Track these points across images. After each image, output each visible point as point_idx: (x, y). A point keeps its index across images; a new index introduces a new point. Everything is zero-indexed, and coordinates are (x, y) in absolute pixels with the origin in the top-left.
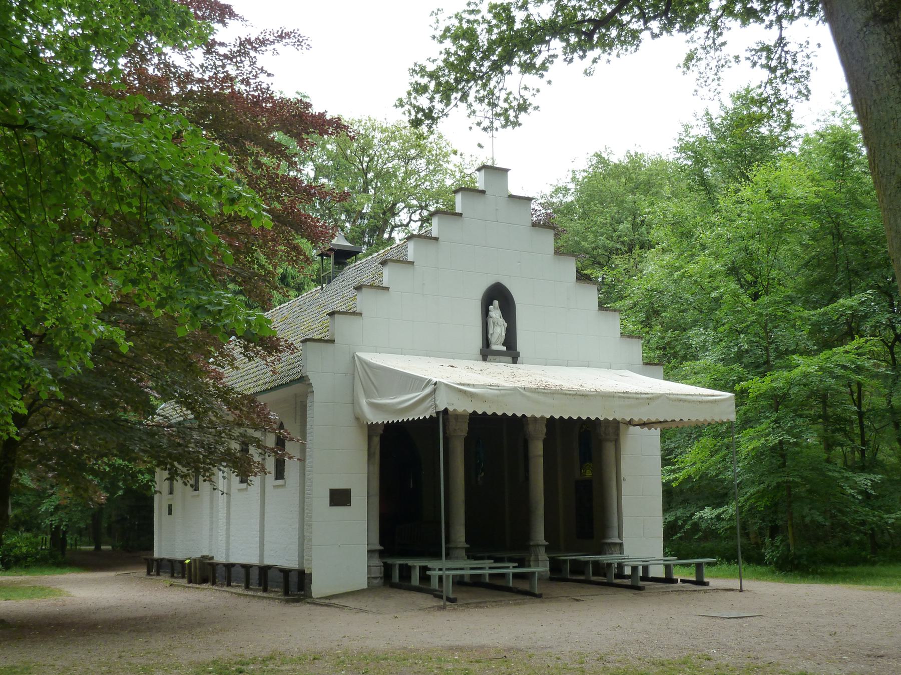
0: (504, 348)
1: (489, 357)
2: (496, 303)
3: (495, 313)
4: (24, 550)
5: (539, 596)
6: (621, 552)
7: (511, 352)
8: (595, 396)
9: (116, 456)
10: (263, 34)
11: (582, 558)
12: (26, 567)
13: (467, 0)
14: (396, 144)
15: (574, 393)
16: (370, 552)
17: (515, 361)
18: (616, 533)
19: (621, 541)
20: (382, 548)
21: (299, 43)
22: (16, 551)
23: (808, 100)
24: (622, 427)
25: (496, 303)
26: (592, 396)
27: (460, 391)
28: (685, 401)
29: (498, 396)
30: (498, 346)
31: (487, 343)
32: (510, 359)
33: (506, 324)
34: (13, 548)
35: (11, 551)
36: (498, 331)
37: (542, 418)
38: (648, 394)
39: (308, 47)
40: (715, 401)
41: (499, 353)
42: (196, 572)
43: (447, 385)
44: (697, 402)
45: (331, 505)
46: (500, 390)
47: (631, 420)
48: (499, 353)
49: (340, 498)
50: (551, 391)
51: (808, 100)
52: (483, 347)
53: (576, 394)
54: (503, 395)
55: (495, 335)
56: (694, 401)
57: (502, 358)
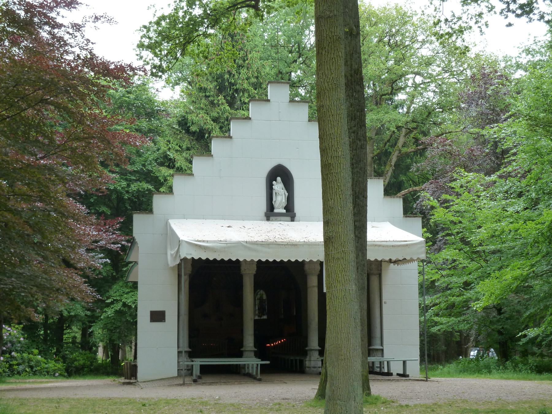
0: (284, 211)
1: (271, 218)
2: (279, 179)
3: (278, 186)
4: (81, 362)
5: (260, 380)
6: (383, 356)
8: (303, 245)
9: (520, 284)
10: (85, 19)
12: (83, 375)
15: (286, 243)
16: (179, 353)
17: (293, 220)
18: (378, 341)
19: (381, 348)
20: (190, 350)
21: (110, 20)
22: (76, 363)
24: (383, 264)
25: (279, 179)
26: (300, 245)
27: (196, 245)
28: (380, 246)
29: (225, 248)
30: (279, 209)
31: (271, 207)
32: (289, 218)
33: (287, 194)
34: (74, 361)
35: (73, 363)
36: (280, 200)
37: (252, 261)
38: (406, 241)
39: (116, 23)
40: (407, 245)
41: (280, 215)
43: (186, 242)
44: (390, 246)
45: (151, 321)
46: (227, 244)
47: (390, 260)
48: (280, 215)
50: (268, 243)
52: (267, 211)
53: (287, 245)
54: (229, 247)
55: (277, 202)
56: (387, 246)
57: (282, 218)
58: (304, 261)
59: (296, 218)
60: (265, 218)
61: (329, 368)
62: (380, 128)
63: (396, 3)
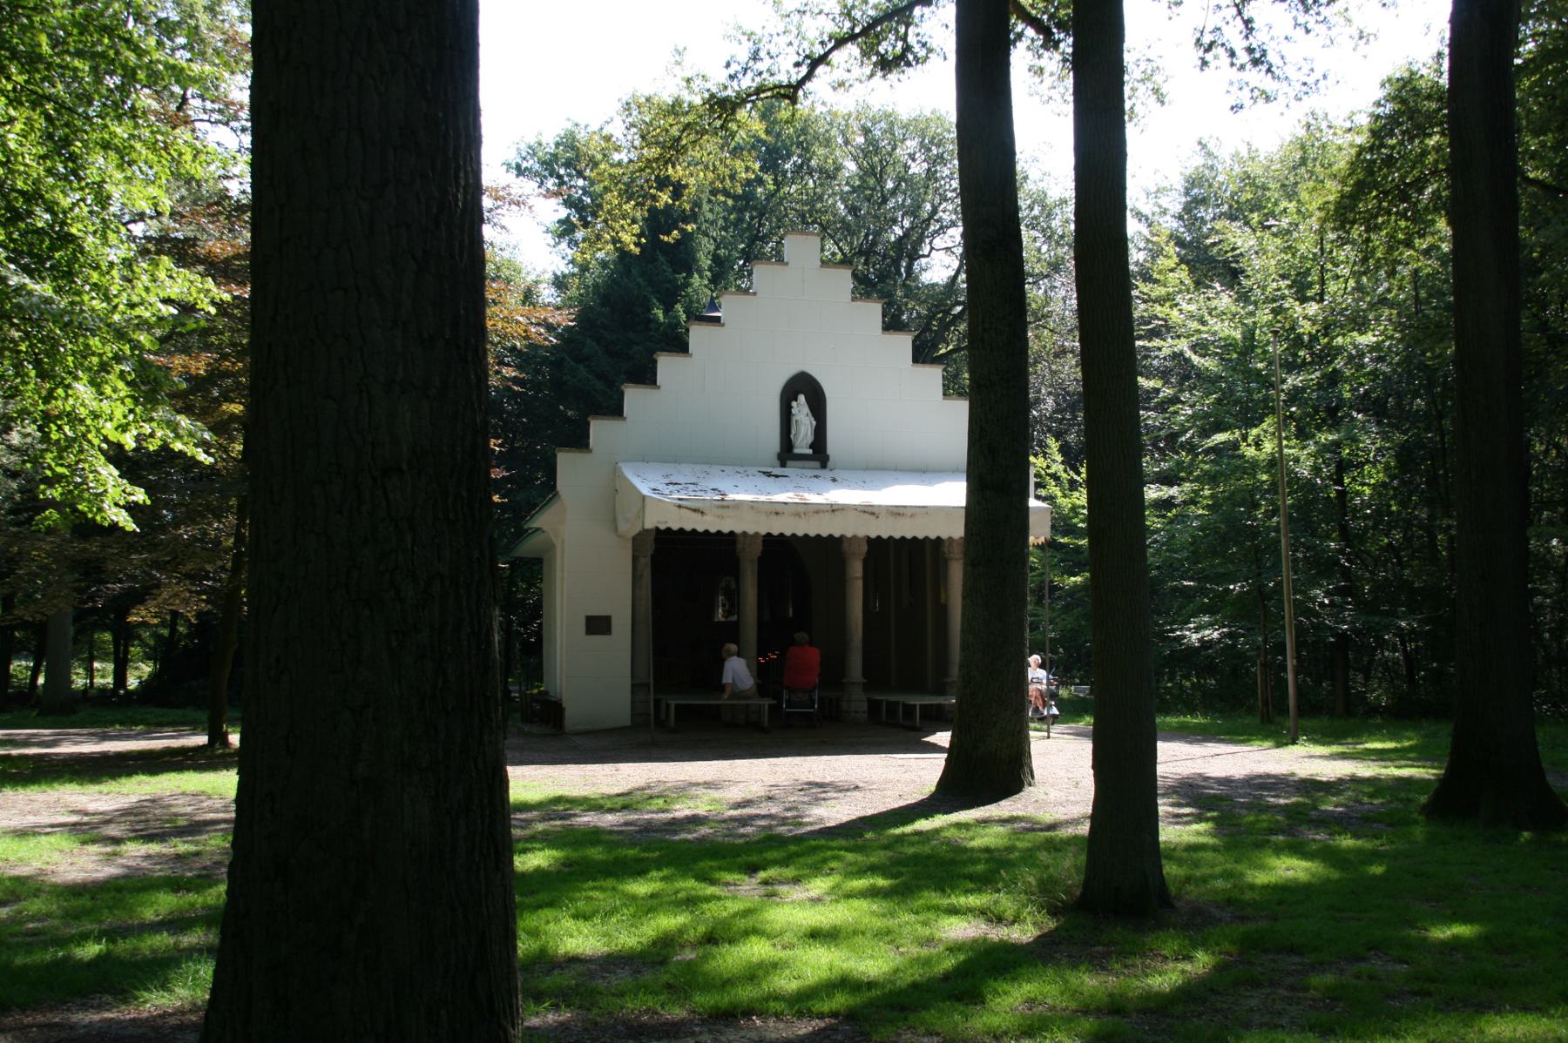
0: (810, 451)
1: (789, 463)
2: (802, 398)
3: (801, 408)
7: (819, 454)
11: (878, 698)
13: (805, 1)
14: (1436, 138)
17: (824, 465)
23: (1202, 70)
25: (802, 398)
32: (817, 464)
33: (814, 423)
42: (1381, 755)
49: (598, 625)
51: (1202, 70)
57: (807, 463)
58: (842, 537)
59: (830, 464)
60: (777, 463)
61: (1281, 872)
62: (616, 249)
63: (1231, 113)
